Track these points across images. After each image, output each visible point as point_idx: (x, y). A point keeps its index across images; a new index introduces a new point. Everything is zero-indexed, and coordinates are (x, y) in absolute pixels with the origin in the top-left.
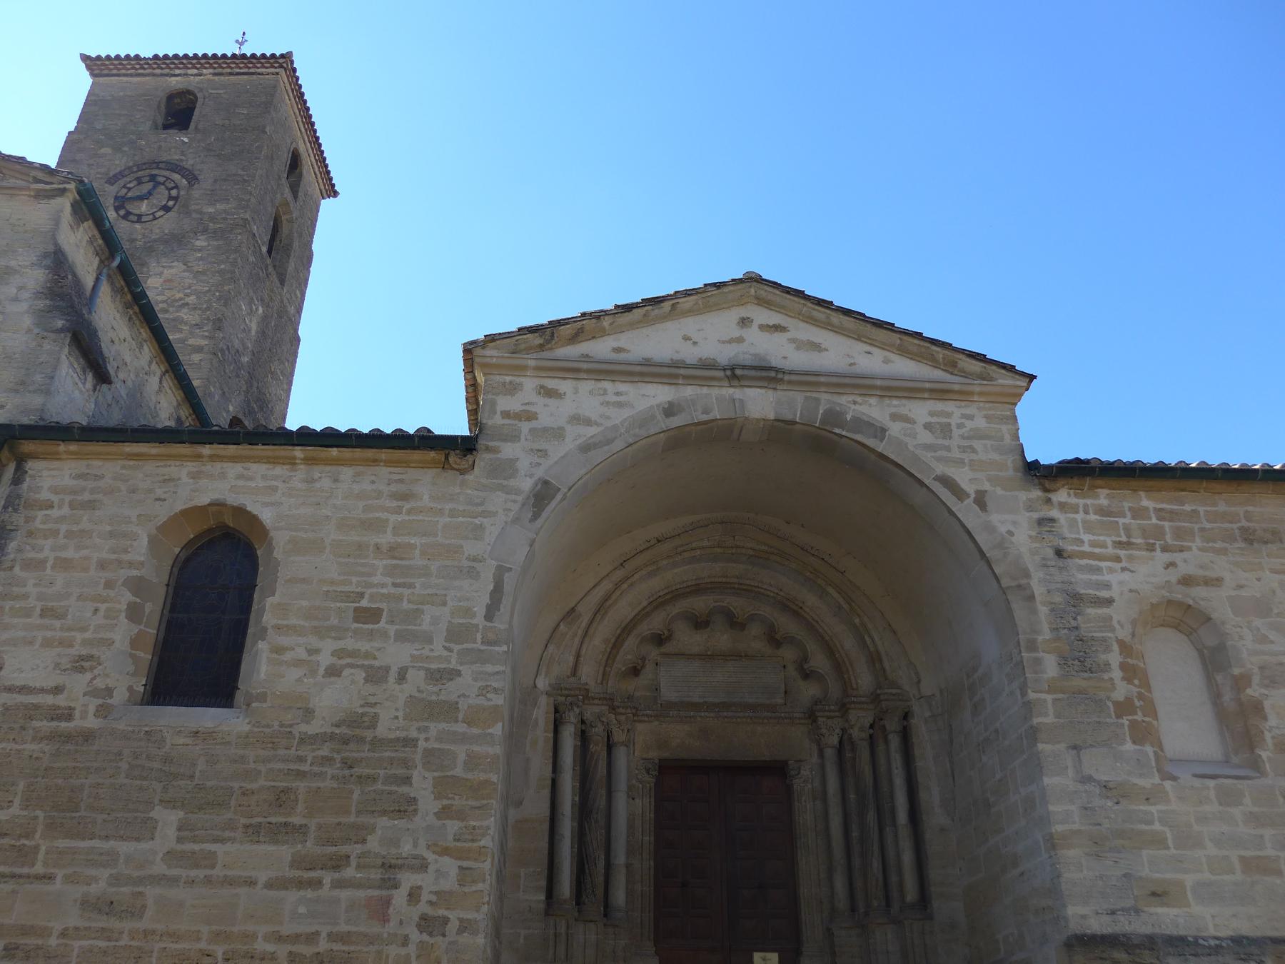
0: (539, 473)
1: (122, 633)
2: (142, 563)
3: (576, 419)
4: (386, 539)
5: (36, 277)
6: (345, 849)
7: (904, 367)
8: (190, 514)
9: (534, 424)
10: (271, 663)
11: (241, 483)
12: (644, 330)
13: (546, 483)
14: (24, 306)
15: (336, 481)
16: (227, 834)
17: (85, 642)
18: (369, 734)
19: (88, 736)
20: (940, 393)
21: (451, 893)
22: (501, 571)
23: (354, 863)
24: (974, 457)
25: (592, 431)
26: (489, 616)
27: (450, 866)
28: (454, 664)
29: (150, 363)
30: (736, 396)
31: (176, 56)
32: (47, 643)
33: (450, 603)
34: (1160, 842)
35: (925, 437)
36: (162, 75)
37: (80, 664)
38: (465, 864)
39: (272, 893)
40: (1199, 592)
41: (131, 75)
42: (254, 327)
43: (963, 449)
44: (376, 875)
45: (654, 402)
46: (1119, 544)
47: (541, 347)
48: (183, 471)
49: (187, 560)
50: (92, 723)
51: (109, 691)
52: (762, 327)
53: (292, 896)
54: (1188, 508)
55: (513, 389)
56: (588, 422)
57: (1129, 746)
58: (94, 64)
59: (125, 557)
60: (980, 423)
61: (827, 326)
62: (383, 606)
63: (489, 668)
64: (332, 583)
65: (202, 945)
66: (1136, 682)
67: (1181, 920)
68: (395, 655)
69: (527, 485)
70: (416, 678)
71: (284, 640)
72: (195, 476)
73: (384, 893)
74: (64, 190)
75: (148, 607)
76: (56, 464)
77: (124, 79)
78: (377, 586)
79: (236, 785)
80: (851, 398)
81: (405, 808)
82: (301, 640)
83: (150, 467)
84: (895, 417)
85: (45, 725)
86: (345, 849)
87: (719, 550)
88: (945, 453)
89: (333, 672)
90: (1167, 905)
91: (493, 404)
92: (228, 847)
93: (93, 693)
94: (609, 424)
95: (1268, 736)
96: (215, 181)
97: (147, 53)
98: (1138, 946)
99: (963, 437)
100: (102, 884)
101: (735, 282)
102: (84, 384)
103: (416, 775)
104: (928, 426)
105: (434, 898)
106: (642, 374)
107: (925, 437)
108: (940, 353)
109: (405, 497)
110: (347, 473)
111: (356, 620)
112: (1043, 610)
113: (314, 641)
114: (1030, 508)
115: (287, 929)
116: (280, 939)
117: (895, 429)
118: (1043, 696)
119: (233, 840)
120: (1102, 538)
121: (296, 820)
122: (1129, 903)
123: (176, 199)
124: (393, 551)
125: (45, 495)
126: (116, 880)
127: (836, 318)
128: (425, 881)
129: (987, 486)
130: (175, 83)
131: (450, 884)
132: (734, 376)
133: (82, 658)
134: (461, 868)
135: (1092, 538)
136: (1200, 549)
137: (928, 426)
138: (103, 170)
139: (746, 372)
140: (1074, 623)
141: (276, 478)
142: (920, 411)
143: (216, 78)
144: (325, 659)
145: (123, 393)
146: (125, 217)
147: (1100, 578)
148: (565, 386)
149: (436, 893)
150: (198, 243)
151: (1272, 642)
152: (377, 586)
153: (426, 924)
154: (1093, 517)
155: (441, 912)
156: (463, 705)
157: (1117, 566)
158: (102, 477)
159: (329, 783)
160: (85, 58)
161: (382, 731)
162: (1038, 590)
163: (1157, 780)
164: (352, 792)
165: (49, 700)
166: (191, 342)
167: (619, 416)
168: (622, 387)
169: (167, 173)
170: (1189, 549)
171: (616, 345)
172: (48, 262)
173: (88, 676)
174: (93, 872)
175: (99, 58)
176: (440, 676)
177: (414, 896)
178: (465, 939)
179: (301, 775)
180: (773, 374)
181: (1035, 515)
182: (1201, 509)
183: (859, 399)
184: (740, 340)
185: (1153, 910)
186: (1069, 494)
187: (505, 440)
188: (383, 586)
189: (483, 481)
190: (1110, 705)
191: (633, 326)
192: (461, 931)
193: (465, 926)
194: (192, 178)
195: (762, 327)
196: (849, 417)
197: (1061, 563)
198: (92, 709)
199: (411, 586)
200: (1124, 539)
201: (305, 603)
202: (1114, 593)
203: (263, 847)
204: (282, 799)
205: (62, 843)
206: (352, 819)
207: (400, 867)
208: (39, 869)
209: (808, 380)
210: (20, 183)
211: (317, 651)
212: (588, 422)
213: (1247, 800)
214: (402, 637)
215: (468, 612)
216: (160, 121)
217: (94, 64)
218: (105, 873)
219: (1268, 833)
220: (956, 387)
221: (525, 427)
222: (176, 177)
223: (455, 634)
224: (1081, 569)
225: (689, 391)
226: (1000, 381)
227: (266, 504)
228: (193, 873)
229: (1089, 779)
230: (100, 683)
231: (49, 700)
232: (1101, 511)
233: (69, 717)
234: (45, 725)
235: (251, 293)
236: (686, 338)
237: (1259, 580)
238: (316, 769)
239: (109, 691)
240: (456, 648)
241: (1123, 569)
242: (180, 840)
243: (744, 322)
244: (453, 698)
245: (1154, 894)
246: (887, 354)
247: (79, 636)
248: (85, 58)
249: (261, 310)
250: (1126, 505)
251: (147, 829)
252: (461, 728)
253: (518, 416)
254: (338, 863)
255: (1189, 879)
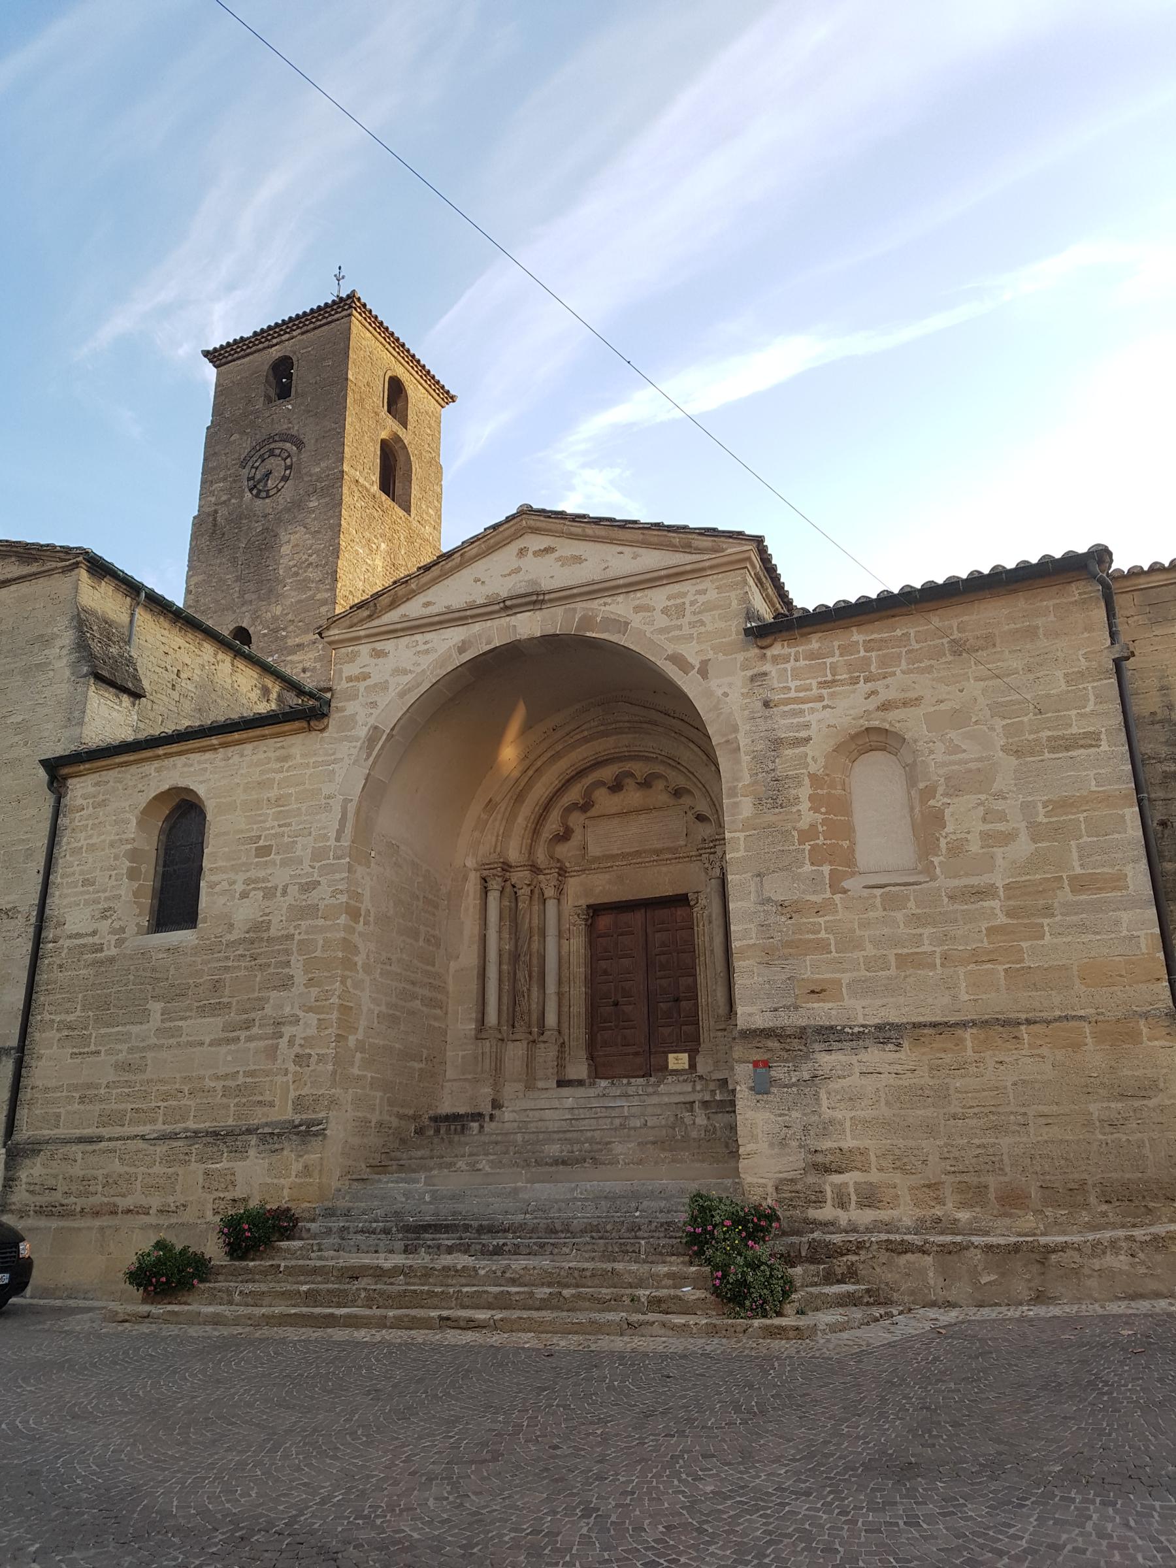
0: (372, 721)
1: (126, 889)
2: (133, 839)
3: (399, 671)
4: (273, 794)
5: (68, 638)
6: (253, 1015)
7: (652, 560)
8: (161, 797)
9: (369, 682)
10: (216, 894)
11: (186, 769)
12: (445, 582)
13: (376, 728)
14: (65, 661)
15: (242, 756)
16: (188, 1014)
17: (107, 899)
18: (265, 935)
19: (112, 960)
20: (676, 576)
21: (313, 1037)
22: (346, 801)
23: (257, 1024)
24: (702, 629)
25: (410, 677)
26: (338, 839)
27: (313, 1018)
28: (316, 877)
29: (216, 655)
30: (513, 623)
31: (270, 328)
32: (87, 903)
33: (313, 833)
34: (823, 947)
35: (662, 621)
36: (264, 348)
37: (105, 914)
38: (322, 1016)
39: (213, 1049)
40: (893, 715)
41: (243, 357)
42: (379, 563)
43: (692, 625)
44: (269, 1030)
45: (451, 643)
46: (823, 684)
47: (370, 617)
48: (150, 768)
49: (171, 829)
50: (113, 951)
51: (122, 930)
52: (536, 554)
53: (224, 1049)
54: (899, 632)
55: (352, 658)
56: (405, 672)
57: (808, 868)
58: (215, 356)
59: (124, 836)
60: (712, 595)
61: (585, 538)
62: (273, 842)
63: (338, 876)
64: (242, 831)
65: (177, 1086)
66: (823, 810)
67: (834, 1012)
68: (281, 877)
69: (362, 732)
70: (293, 890)
71: (214, 878)
72: (158, 770)
73: (275, 1041)
74: (77, 563)
75: (144, 868)
76: (83, 778)
77: (238, 362)
78: (268, 829)
79: (191, 981)
80: (602, 601)
81: (286, 983)
82: (225, 876)
83: (133, 769)
84: (638, 609)
85: (89, 957)
86: (253, 1015)
87: (602, 728)
88: (677, 633)
89: (244, 895)
90: (823, 1001)
91: (341, 671)
92: (189, 1022)
93: (113, 932)
94: (419, 669)
95: (943, 842)
96: (317, 440)
97: (248, 334)
98: (789, 1036)
99: (694, 613)
100: (124, 1053)
101: (509, 519)
102: (120, 705)
103: (293, 959)
104: (665, 611)
105: (303, 1042)
106: (440, 622)
107: (662, 621)
108: (676, 538)
109: (285, 759)
110: (248, 748)
111: (257, 856)
112: (745, 759)
113: (232, 876)
114: (744, 668)
115: (221, 1071)
116: (218, 1078)
117: (636, 621)
118: (737, 834)
119: (191, 1017)
120: (808, 682)
121: (225, 1000)
122: (789, 1001)
123: (290, 467)
124: (279, 801)
125: (79, 801)
126: (131, 1050)
127: (590, 530)
128: (298, 1031)
129: (711, 655)
130: (275, 353)
131: (312, 1031)
132: (507, 608)
133: (105, 910)
134: (319, 1020)
135: (798, 683)
136: (903, 672)
137: (665, 611)
138: (236, 456)
139: (514, 602)
140: (771, 766)
141: (205, 761)
142: (658, 597)
143: (304, 336)
144: (239, 887)
145: (191, 687)
146: (257, 496)
147: (802, 720)
148: (388, 646)
149: (304, 1038)
150: (311, 505)
151: (965, 751)
152: (268, 829)
153: (300, 1059)
154: (802, 663)
155: (308, 1051)
156: (321, 907)
157: (819, 705)
158: (108, 782)
159: (243, 973)
160: (206, 354)
161: (273, 932)
162: (743, 740)
163: (828, 895)
164: (256, 976)
165: (90, 940)
166: (318, 597)
167: (426, 662)
168: (428, 636)
169: (280, 445)
170: (894, 674)
171: (425, 600)
172: (75, 623)
173: (110, 921)
174: (118, 1047)
175: (215, 350)
176: (309, 887)
177: (291, 1042)
178: (321, 1067)
179: (227, 968)
180: (534, 598)
181: (749, 673)
182: (912, 631)
183: (609, 600)
184: (518, 570)
185: (810, 1005)
186: (783, 646)
187: (349, 700)
188: (273, 828)
189: (335, 735)
190: (795, 834)
191: (435, 581)
192: (319, 1061)
193: (321, 1059)
194: (299, 444)
195: (536, 554)
196: (598, 619)
197: (767, 712)
198: (113, 943)
199: (290, 825)
200: (829, 678)
201: (227, 849)
202: (812, 732)
203: (208, 1020)
204: (216, 986)
205: (102, 1031)
206: (256, 995)
207: (283, 1024)
208: (93, 1048)
209: (566, 596)
210: (54, 564)
211: (234, 882)
212: (405, 672)
213: (911, 904)
214: (284, 863)
215: (325, 837)
216: (272, 393)
217: (215, 356)
218: (125, 1047)
219: (927, 931)
220: (707, 564)
221: (362, 686)
222: (288, 445)
223: (318, 855)
224: (784, 715)
225: (477, 628)
226: (729, 551)
227: (201, 782)
228: (171, 1041)
229: (769, 900)
230: (116, 925)
231: (90, 940)
232: (812, 656)
233: (102, 950)
234: (89, 957)
235: (367, 535)
236: (477, 580)
237: (961, 691)
238: (236, 964)
239: (122, 930)
240: (317, 865)
241: (824, 707)
242: (163, 1021)
243: (522, 552)
244: (316, 902)
245: (813, 992)
246: (635, 549)
247: (102, 895)
248: (206, 354)
249: (383, 546)
250: (836, 644)
251: (144, 1015)
252: (321, 922)
253: (357, 679)
254: (248, 1025)
255: (846, 978)
